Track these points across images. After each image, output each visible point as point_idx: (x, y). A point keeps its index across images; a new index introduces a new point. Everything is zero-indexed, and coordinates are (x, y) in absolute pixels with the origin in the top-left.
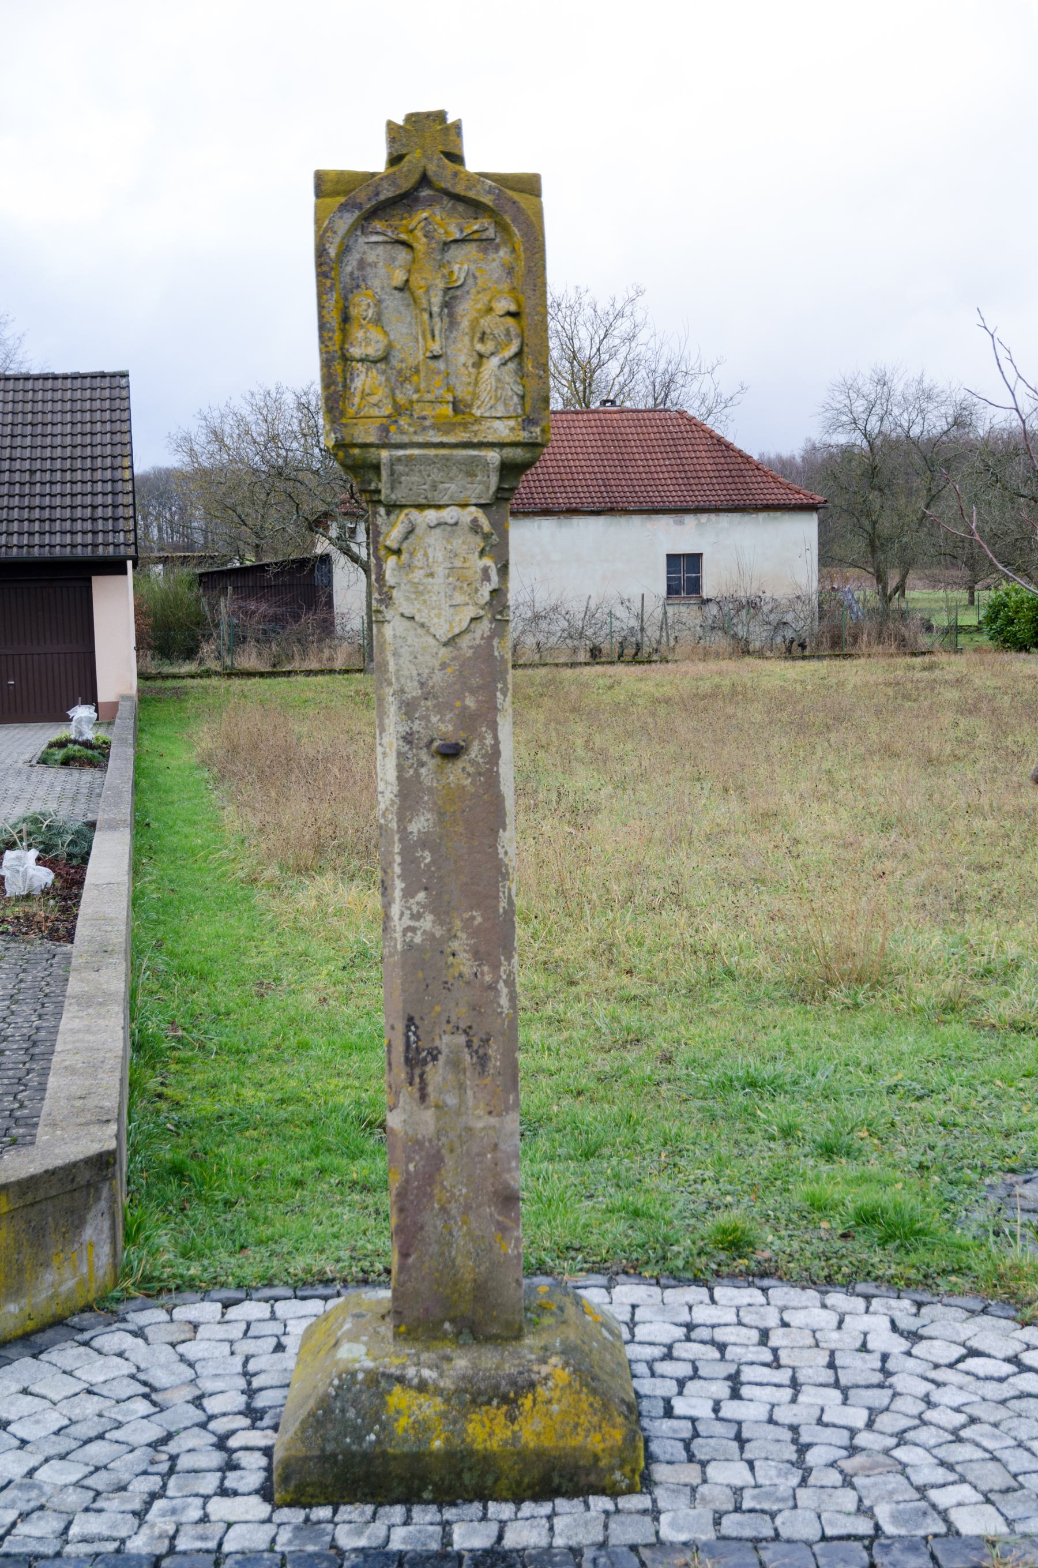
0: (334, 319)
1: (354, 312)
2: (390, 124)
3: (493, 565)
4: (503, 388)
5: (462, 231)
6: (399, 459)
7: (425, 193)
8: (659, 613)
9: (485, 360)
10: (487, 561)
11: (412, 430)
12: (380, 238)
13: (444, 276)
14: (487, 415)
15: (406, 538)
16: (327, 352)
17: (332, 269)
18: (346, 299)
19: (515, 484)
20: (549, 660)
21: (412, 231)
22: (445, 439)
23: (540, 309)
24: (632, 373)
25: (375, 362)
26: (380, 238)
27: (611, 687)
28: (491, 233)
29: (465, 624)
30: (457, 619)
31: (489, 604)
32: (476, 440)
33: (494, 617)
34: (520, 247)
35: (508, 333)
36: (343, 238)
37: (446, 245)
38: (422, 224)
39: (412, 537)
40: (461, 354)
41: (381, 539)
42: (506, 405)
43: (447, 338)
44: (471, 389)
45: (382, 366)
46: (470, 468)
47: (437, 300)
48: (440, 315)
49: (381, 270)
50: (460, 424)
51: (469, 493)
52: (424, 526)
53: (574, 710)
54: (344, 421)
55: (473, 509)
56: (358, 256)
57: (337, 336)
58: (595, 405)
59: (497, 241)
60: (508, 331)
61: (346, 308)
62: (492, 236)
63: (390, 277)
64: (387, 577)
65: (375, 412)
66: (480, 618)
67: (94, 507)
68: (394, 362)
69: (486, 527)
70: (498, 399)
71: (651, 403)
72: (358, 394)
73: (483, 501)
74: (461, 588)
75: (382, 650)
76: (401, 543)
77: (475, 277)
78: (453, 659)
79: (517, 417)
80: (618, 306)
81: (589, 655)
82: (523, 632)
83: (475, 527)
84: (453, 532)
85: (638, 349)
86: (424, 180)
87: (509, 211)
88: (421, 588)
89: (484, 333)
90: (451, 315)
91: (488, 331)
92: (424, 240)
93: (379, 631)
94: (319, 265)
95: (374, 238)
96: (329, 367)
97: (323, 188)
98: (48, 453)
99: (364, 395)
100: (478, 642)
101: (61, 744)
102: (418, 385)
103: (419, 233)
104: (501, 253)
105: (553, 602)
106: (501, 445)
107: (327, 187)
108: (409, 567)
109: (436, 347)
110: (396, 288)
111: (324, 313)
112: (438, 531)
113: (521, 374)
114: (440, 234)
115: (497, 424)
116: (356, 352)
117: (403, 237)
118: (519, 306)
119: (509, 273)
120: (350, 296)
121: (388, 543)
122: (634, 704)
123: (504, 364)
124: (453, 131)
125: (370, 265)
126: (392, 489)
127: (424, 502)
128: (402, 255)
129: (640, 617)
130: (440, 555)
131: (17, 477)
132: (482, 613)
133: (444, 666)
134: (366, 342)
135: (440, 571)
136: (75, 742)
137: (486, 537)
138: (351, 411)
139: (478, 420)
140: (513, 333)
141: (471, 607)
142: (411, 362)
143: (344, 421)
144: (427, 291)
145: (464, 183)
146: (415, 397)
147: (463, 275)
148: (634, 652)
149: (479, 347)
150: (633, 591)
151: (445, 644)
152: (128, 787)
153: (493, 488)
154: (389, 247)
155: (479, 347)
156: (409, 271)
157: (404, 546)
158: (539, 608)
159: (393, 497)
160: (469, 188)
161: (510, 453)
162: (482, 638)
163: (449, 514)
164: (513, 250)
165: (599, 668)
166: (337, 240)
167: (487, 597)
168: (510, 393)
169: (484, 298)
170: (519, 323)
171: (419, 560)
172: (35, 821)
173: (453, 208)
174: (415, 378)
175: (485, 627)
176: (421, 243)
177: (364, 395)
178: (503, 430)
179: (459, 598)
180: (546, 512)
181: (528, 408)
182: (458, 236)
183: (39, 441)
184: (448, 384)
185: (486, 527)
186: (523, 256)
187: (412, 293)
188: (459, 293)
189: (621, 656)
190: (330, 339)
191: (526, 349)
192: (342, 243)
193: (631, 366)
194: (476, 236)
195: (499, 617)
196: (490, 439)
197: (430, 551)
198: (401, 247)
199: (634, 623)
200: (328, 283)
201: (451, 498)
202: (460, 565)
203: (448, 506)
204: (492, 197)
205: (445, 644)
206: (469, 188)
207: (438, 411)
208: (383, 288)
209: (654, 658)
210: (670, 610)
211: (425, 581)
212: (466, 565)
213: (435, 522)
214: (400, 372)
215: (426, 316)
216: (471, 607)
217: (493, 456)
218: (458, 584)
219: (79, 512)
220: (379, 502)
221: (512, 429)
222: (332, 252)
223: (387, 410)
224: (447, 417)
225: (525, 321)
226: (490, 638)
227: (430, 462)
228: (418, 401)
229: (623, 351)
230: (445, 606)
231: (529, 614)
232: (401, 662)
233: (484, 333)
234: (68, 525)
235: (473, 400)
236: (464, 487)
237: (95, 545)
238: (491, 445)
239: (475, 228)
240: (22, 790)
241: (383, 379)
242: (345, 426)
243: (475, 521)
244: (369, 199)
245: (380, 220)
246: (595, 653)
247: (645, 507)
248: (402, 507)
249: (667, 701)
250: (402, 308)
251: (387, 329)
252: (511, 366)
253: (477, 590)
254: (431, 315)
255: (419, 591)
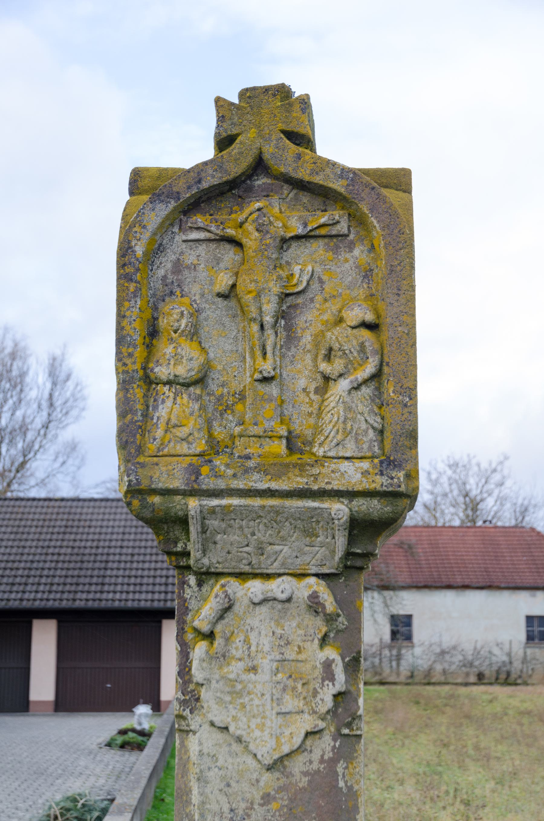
0: (137, 331)
1: (163, 323)
2: (219, 102)
3: (338, 659)
4: (354, 419)
5: (305, 225)
6: (213, 511)
7: (261, 181)
8: (521, 653)
9: (331, 383)
10: (331, 653)
11: (230, 472)
12: (202, 235)
13: (280, 278)
14: (331, 454)
15: (221, 617)
16: (124, 372)
17: (138, 270)
18: (155, 308)
19: (370, 548)
20: (451, 680)
21: (241, 225)
22: (274, 485)
23: (405, 318)
24: (502, 505)
25: (187, 385)
26: (202, 235)
27: (491, 701)
28: (343, 227)
29: (297, 741)
30: (287, 733)
31: (333, 712)
32: (316, 487)
33: (338, 730)
34: (380, 243)
35: (362, 348)
36: (154, 234)
37: (285, 242)
38: (255, 216)
39: (229, 616)
40: (301, 376)
41: (189, 618)
42: (357, 441)
43: (283, 356)
44: (312, 421)
45: (197, 390)
46: (309, 526)
47: (270, 308)
48: (275, 325)
49: (202, 274)
50: (295, 466)
51: (307, 558)
52: (246, 601)
53: (468, 717)
54: (141, 459)
55: (312, 580)
56: (173, 257)
57: (139, 352)
58: (480, 523)
59: (352, 237)
60: (362, 346)
61: (155, 319)
62: (345, 231)
63: (212, 283)
64: (193, 671)
65: (183, 448)
66: (320, 731)
67: (167, 577)
68: (213, 386)
69: (330, 605)
70: (346, 434)
71: (513, 523)
72: (162, 426)
73: (326, 570)
74: (294, 689)
75: (185, 772)
76: (215, 624)
77: (321, 281)
78: (280, 789)
79: (373, 457)
80: (494, 466)
81: (476, 678)
82: (435, 662)
83: (314, 605)
84: (285, 611)
85: (505, 491)
86: (259, 165)
87: (371, 211)
88: (239, 687)
89: (330, 349)
90: (289, 328)
91: (336, 346)
92: (257, 234)
93: (182, 744)
94: (121, 265)
95: (194, 235)
96: (127, 390)
97: (140, 184)
98: (143, 544)
99: (169, 427)
100: (315, 766)
101: (123, 732)
102: (243, 414)
103: (250, 227)
104: (357, 252)
105: (453, 643)
106: (351, 495)
107: (145, 183)
108: (224, 657)
109: (267, 367)
110: (219, 295)
111: (124, 323)
112: (264, 609)
113: (380, 402)
114: (278, 229)
115: (345, 466)
116: (162, 372)
117: (230, 232)
118: (378, 317)
119: (365, 277)
120: (161, 305)
121: (196, 623)
122: (506, 714)
123: (357, 388)
124: (297, 107)
125: (188, 267)
126: (204, 552)
127: (247, 569)
128: (230, 255)
129: (509, 654)
130: (266, 642)
131: (123, 558)
132: (322, 725)
133: (267, 799)
134: (176, 359)
135: (266, 664)
136: (134, 730)
137: (330, 619)
138: (152, 447)
139: (319, 461)
140: (369, 349)
141: (306, 716)
142: (235, 386)
143: (141, 459)
144: (258, 296)
145: (309, 167)
146: (237, 430)
147: (305, 278)
148: (505, 678)
149: (324, 366)
150: (505, 637)
151: (269, 768)
152: (147, 773)
153: (339, 554)
154: (213, 246)
155: (324, 366)
156: (237, 274)
157: (219, 628)
158: (445, 646)
159: (206, 561)
160: (314, 172)
161: (362, 505)
162: (322, 761)
163: (279, 587)
164: (372, 248)
165: (482, 688)
166: (147, 235)
167: (329, 703)
168: (364, 426)
169: (333, 307)
170: (378, 337)
171: (237, 648)
172: (75, 800)
173: (296, 198)
174: (239, 407)
175: (326, 745)
176: (251, 238)
177: (169, 427)
178: (352, 475)
179: (290, 703)
180: (449, 587)
181: (388, 446)
182: (300, 231)
183: (139, 537)
184: (282, 415)
185: (330, 605)
186: (383, 253)
187: (239, 301)
188: (300, 300)
189: (497, 679)
190: (130, 355)
191: (386, 369)
192: (152, 240)
193: (502, 500)
194: (323, 231)
195: (346, 731)
196: (335, 485)
197: (253, 636)
198: (228, 246)
199: (505, 658)
200: (132, 287)
201: (283, 564)
202: (293, 656)
203: (280, 575)
204: (345, 182)
205: (269, 768)
206: (314, 172)
207: (267, 448)
208: (202, 295)
209: (519, 681)
210: (529, 651)
211: (244, 677)
212: (301, 657)
213: (260, 597)
214: (219, 399)
215: (255, 327)
216: (306, 716)
217: (340, 509)
218: (290, 683)
219: (158, 580)
220: (188, 568)
221: (365, 473)
222: (139, 250)
223: (200, 446)
224: (278, 456)
225: (386, 333)
226: (333, 761)
227: (256, 515)
228: (241, 436)
229: (496, 492)
230: (271, 714)
231: (438, 650)
232: (208, 790)
233: (330, 349)
234: (150, 588)
235: (314, 435)
236: (300, 550)
237: (166, 601)
238: (337, 494)
239: (322, 220)
240: (86, 768)
241: (197, 406)
242: (143, 465)
243: (314, 596)
244: (189, 188)
245: (204, 214)
246: (480, 676)
247: (511, 585)
248: (219, 575)
249: (529, 713)
250: (226, 320)
251: (205, 345)
252: (366, 391)
253: (315, 693)
254: (262, 327)
255: (235, 691)
